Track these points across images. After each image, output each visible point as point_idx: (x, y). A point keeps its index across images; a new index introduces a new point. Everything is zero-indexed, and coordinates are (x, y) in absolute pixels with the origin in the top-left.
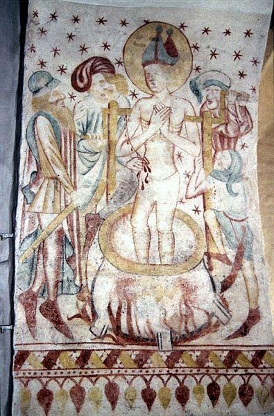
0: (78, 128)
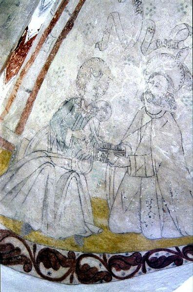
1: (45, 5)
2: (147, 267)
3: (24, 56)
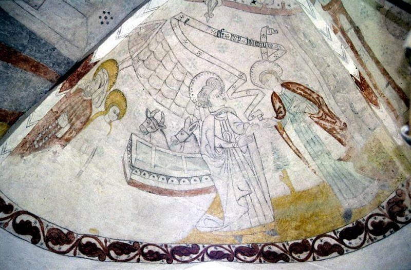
0: (334, 172)
1: (342, 55)
2: (206, 257)
3: (368, 86)
